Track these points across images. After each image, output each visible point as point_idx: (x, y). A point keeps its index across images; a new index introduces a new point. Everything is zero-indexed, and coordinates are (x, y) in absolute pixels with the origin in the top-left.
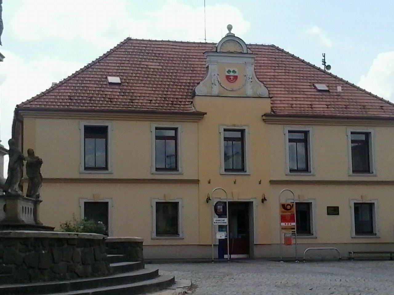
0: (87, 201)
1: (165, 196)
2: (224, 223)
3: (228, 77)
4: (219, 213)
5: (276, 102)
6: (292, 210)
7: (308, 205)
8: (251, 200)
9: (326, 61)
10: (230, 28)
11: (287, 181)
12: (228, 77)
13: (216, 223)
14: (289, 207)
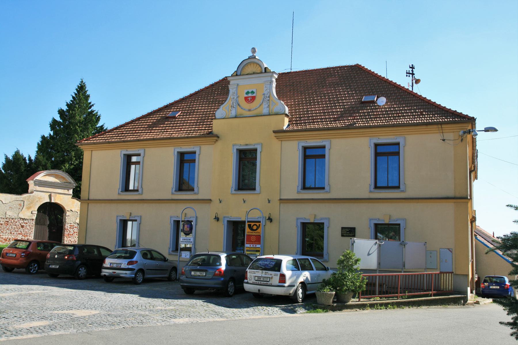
4: (186, 232)
6: (258, 231)
7: (320, 226)
9: (414, 72)
12: (246, 99)
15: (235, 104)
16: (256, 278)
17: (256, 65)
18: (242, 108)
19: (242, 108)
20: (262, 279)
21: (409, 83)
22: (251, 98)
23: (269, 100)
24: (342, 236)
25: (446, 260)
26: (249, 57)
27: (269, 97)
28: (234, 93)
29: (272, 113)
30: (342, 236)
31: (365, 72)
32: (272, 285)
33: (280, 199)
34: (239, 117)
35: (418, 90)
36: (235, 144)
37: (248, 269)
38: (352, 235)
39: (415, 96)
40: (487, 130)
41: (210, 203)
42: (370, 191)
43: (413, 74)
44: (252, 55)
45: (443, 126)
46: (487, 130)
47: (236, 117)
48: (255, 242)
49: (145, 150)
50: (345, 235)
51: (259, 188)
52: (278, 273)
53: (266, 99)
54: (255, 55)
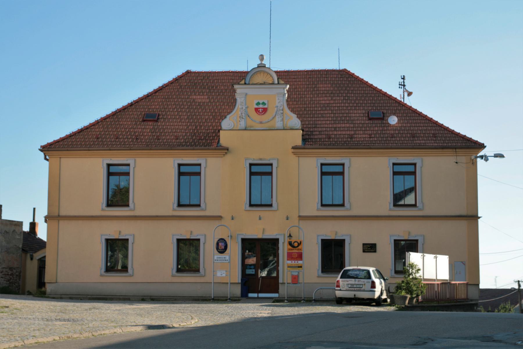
0: (243, 237)
1: (336, 233)
2: (225, 260)
3: (256, 110)
4: (220, 250)
5: (314, 133)
6: (300, 247)
8: (277, 237)
9: (405, 84)
10: (262, 57)
11: (317, 217)
12: (256, 110)
13: (217, 260)
14: (296, 244)
15: (244, 115)
16: (350, 286)
17: (266, 75)
18: (252, 120)
19: (252, 120)
20: (355, 286)
21: (401, 95)
22: (263, 110)
23: (282, 113)
24: (364, 251)
25: (460, 272)
26: (258, 65)
27: (282, 110)
28: (243, 103)
29: (286, 127)
30: (364, 251)
31: (357, 80)
32: (365, 290)
33: (299, 216)
34: (249, 129)
35: (409, 101)
36: (247, 158)
37: (341, 278)
38: (373, 251)
39: (404, 105)
40: (496, 156)
41: (221, 220)
42: (390, 209)
43: (404, 86)
44: (259, 62)
45: (457, 150)
46: (496, 156)
47: (245, 129)
48: (296, 258)
49: (135, 160)
50: (366, 251)
51: (276, 204)
52: (370, 281)
53: (279, 112)
54: (263, 62)
